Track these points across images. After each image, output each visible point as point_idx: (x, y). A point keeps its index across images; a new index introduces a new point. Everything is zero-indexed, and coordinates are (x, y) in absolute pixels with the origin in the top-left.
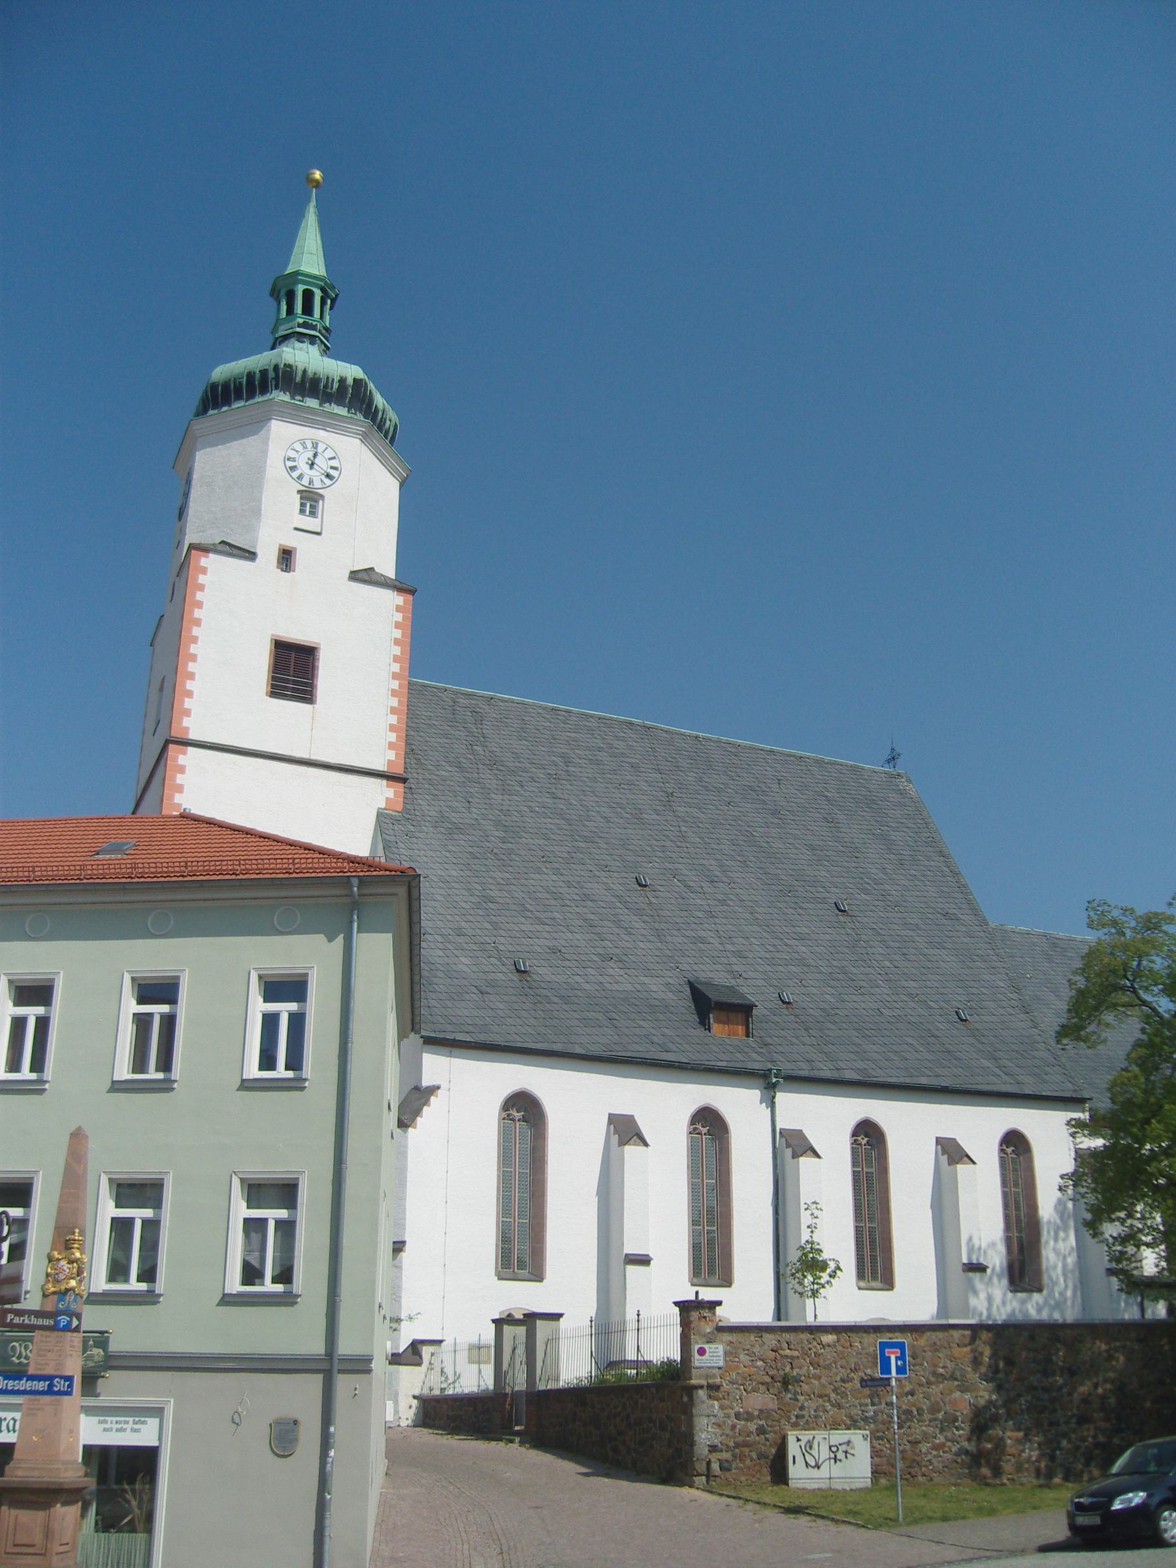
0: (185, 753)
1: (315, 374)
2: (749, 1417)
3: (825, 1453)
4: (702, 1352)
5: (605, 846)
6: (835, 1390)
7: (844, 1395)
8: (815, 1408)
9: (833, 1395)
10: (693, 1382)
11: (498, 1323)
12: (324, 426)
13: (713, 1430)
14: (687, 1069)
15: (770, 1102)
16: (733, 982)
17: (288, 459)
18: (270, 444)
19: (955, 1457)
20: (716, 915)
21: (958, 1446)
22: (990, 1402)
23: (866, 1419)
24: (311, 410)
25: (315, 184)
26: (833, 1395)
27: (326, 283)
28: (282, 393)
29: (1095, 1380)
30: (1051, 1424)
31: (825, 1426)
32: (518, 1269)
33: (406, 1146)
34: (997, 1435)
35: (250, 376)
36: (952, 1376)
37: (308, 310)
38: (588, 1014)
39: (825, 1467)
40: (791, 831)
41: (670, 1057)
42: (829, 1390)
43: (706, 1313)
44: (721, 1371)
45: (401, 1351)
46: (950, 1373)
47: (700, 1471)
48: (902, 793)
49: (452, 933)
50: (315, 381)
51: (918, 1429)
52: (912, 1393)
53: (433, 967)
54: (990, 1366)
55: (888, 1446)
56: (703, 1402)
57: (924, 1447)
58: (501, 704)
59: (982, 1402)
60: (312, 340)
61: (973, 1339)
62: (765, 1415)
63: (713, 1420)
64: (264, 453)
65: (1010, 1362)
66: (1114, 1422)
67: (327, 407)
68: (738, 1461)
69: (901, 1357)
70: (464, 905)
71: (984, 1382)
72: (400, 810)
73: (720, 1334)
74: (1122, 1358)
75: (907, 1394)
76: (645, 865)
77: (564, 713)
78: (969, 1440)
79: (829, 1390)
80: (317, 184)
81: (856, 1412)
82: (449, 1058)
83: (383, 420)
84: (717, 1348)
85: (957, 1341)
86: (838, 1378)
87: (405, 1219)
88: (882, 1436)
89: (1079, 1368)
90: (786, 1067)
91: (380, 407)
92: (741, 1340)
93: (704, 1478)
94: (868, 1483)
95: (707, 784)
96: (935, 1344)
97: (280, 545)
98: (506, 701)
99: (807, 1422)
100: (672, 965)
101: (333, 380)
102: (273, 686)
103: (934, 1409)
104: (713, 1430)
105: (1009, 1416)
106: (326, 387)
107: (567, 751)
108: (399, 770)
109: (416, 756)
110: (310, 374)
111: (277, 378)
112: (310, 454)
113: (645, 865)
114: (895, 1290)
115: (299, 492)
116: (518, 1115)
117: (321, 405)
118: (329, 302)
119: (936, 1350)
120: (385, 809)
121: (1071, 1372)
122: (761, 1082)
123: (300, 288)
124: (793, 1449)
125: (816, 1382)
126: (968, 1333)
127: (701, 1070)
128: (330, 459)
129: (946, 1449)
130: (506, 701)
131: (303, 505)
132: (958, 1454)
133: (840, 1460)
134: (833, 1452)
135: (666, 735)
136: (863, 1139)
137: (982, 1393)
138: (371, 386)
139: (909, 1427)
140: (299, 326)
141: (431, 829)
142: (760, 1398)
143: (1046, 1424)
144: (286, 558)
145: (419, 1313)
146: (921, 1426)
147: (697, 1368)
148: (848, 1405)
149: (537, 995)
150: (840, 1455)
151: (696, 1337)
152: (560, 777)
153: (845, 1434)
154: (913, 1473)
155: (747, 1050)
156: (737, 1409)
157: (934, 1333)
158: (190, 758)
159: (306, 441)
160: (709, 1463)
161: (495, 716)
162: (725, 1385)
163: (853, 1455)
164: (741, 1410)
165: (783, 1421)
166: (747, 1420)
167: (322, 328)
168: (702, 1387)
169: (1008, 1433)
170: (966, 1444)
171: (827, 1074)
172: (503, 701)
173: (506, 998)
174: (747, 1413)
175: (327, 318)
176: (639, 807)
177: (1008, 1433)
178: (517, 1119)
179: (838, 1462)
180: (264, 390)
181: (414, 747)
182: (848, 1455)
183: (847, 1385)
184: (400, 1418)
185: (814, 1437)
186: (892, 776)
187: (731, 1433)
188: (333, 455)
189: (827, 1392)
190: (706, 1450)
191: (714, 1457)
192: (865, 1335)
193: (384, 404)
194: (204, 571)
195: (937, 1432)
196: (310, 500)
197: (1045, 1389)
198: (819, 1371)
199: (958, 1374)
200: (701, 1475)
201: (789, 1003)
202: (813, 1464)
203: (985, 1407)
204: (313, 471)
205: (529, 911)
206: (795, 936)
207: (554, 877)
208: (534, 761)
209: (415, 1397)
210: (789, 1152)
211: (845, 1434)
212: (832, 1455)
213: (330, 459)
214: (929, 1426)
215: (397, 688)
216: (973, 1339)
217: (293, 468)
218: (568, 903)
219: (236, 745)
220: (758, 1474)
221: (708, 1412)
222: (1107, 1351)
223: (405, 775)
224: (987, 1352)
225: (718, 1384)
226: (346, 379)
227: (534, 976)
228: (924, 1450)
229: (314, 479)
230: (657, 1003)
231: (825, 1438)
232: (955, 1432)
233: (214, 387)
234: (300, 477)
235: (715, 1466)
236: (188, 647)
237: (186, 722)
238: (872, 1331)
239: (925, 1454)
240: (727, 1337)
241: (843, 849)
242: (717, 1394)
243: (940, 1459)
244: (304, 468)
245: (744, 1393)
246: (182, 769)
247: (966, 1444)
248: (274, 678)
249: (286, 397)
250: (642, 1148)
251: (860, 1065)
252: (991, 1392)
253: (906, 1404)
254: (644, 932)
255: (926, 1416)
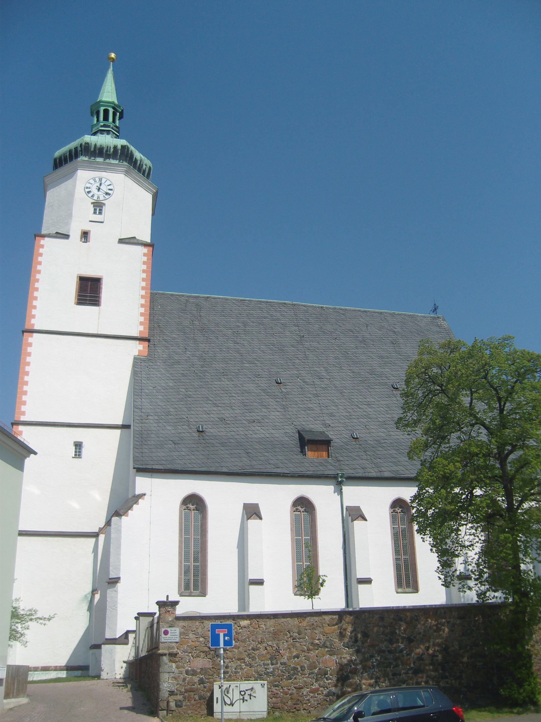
0: (32, 337)
1: (101, 145)
2: (194, 673)
3: (237, 696)
4: (166, 633)
5: (260, 365)
6: (248, 655)
7: (253, 658)
8: (235, 667)
9: (247, 659)
10: (160, 651)
11: (136, 618)
12: (105, 170)
13: (171, 681)
14: (288, 476)
15: (340, 492)
16: (325, 429)
17: (87, 188)
18: (77, 182)
19: (325, 697)
20: (320, 396)
21: (328, 690)
22: (351, 661)
23: (267, 674)
24: (98, 163)
25: (112, 60)
26: (247, 659)
27: (115, 104)
28: (84, 157)
29: (427, 645)
30: (394, 675)
31: (241, 678)
32: (194, 590)
33: (120, 526)
34: (356, 682)
35: (70, 151)
36: (323, 645)
37: (106, 118)
38: (235, 451)
39: (236, 705)
40: (371, 350)
41: (279, 471)
42: (244, 655)
43: (169, 609)
44: (177, 645)
45: (117, 637)
46: (323, 643)
47: (162, 707)
48: (438, 326)
49: (164, 414)
50: (101, 149)
51: (301, 680)
52: (297, 656)
53: (149, 432)
54: (351, 638)
55: (281, 690)
56: (166, 664)
57: (305, 691)
58: (213, 300)
59: (345, 661)
60: (108, 132)
61: (340, 620)
62: (204, 672)
63: (172, 675)
64: (74, 186)
65: (366, 635)
66: (440, 671)
67: (108, 161)
68: (187, 701)
69: (229, 634)
70: (173, 400)
71: (346, 648)
72: (146, 355)
73: (177, 622)
74: (447, 630)
75: (294, 657)
76: (282, 373)
77: (248, 302)
78: (336, 686)
79: (244, 655)
80: (113, 60)
81: (261, 669)
82: (151, 479)
83: (141, 166)
84: (176, 630)
85: (328, 622)
86: (250, 648)
87: (120, 565)
88: (278, 684)
89: (415, 637)
90: (349, 472)
91: (139, 158)
92: (190, 625)
93: (165, 712)
94: (265, 715)
95: (324, 330)
96: (313, 624)
97: (82, 230)
98: (216, 299)
99: (230, 676)
100: (290, 423)
101: (110, 147)
102: (79, 299)
103: (312, 666)
104: (171, 681)
105: (365, 668)
106: (107, 151)
107: (246, 320)
108: (146, 335)
109: (161, 329)
110: (98, 145)
111: (81, 151)
112: (98, 185)
113: (282, 373)
114: (419, 592)
115: (92, 203)
116: (192, 507)
117: (104, 160)
118: (118, 114)
119: (314, 629)
120: (138, 356)
121: (410, 640)
122: (334, 481)
123: (102, 109)
124: (217, 693)
125: (236, 651)
126: (336, 617)
127: (296, 477)
128: (108, 185)
129: (320, 692)
130: (216, 299)
131: (95, 210)
132: (327, 695)
133: (247, 700)
134: (242, 695)
135: (305, 308)
136: (398, 509)
137: (345, 656)
138: (132, 148)
139: (295, 678)
140: (101, 126)
141: (162, 364)
142: (201, 661)
143: (390, 674)
144: (85, 235)
145: (55, 614)
146: (304, 678)
147: (163, 643)
148: (256, 665)
149: (207, 443)
150: (247, 697)
151: (163, 624)
152: (240, 333)
153: (250, 683)
154: (298, 708)
155: (326, 464)
156: (187, 668)
157: (312, 618)
158: (35, 339)
159: (96, 178)
160: (168, 702)
161: (209, 306)
162: (180, 653)
163: (255, 697)
164: (190, 669)
165: (215, 676)
166: (193, 675)
167: (113, 127)
168: (165, 655)
169: (364, 681)
170: (333, 689)
171: (374, 474)
172: (214, 298)
173: (188, 446)
174: (193, 670)
175: (117, 122)
176: (283, 344)
177: (364, 681)
178: (192, 509)
179: (245, 701)
180: (77, 156)
181: (160, 324)
182: (252, 697)
183: (256, 652)
184: (116, 674)
185: (230, 686)
186: (434, 318)
187: (183, 684)
188: (110, 183)
189: (243, 657)
190: (167, 694)
191: (171, 699)
192: (267, 620)
193: (141, 157)
194: (42, 246)
195: (314, 681)
196: (98, 207)
197: (390, 652)
198: (238, 643)
199: (328, 643)
200: (164, 710)
201: (357, 438)
202: (229, 703)
203: (346, 665)
204: (100, 192)
205: (211, 400)
206: (365, 403)
207: (228, 383)
208: (226, 326)
209: (124, 662)
210: (350, 518)
211: (250, 683)
212: (242, 697)
213: (108, 185)
214: (308, 677)
215: (144, 294)
216: (340, 620)
217: (89, 192)
218: (234, 395)
219: (59, 330)
220: (199, 709)
221: (169, 670)
222: (436, 625)
223: (149, 338)
224: (350, 629)
225: (175, 652)
226: (117, 146)
227: (207, 433)
228: (305, 693)
229: (100, 196)
230: (277, 443)
231: (237, 686)
232: (326, 681)
233: (55, 160)
234: (93, 196)
235: (172, 704)
236: (34, 284)
237: (33, 321)
238: (272, 617)
239: (305, 695)
240: (182, 623)
241: (400, 357)
242: (175, 659)
243: (315, 699)
244: (94, 191)
245: (192, 658)
246: (30, 345)
247: (333, 689)
248: (79, 296)
249: (86, 159)
250: (258, 521)
251: (395, 468)
252: (352, 655)
253: (294, 664)
254: (276, 407)
255: (307, 671)
